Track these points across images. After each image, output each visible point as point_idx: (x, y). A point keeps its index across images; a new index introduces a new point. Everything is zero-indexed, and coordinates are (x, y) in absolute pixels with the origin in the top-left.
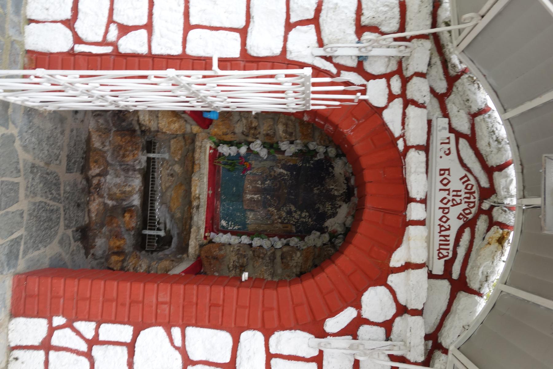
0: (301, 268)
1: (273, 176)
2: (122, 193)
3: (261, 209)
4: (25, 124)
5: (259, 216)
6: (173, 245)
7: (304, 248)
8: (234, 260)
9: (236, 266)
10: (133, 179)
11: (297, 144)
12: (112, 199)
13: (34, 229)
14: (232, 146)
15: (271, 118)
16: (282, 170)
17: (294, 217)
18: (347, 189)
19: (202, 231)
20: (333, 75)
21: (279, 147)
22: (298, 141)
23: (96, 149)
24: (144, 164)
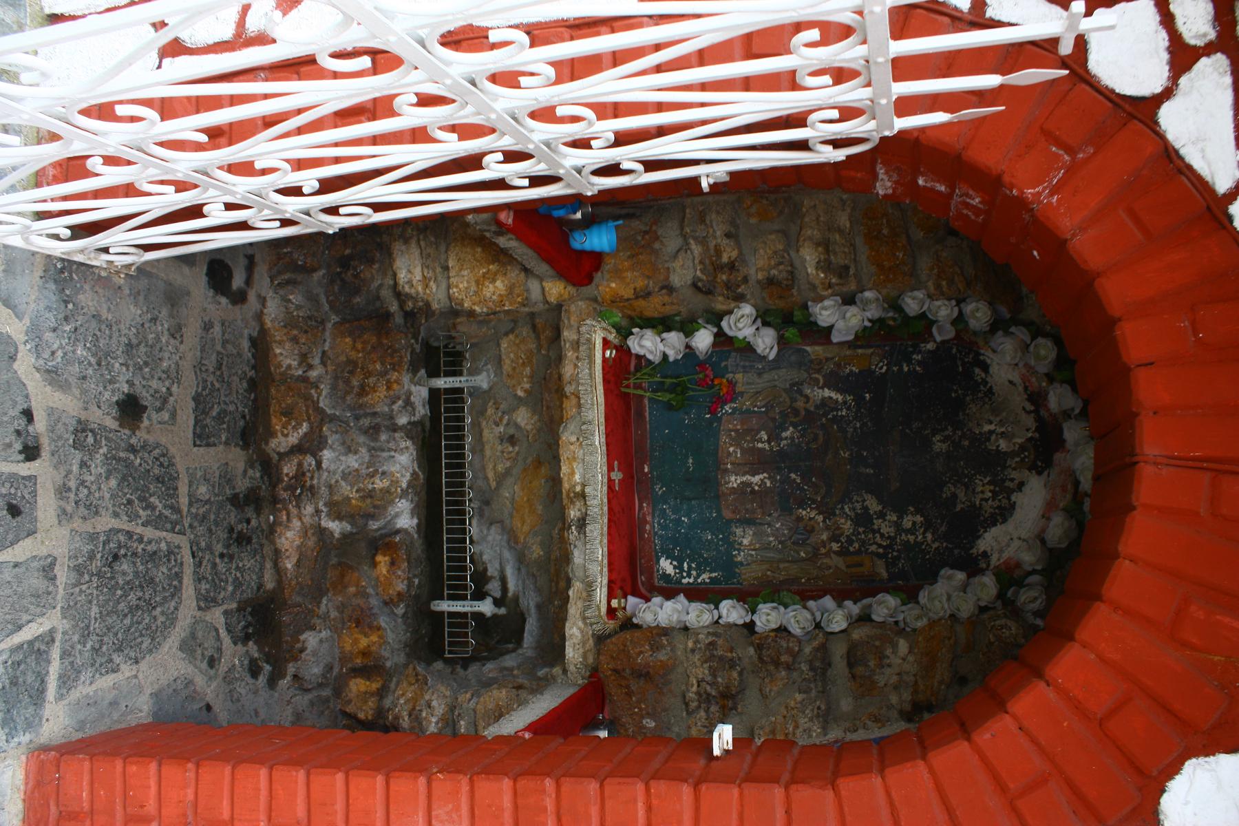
0: (915, 692)
1: (803, 413)
2: (363, 498)
3: (775, 515)
4: (49, 309)
5: (771, 539)
6: (528, 639)
7: (919, 624)
8: (700, 676)
9: (709, 695)
10: (392, 453)
11: (866, 302)
12: (339, 517)
13: (95, 610)
15: (778, 231)
16: (827, 393)
17: (879, 531)
18: (1037, 430)
19: (601, 594)
20: (959, 15)
21: (812, 319)
22: (868, 294)
23: (285, 377)
24: (422, 411)
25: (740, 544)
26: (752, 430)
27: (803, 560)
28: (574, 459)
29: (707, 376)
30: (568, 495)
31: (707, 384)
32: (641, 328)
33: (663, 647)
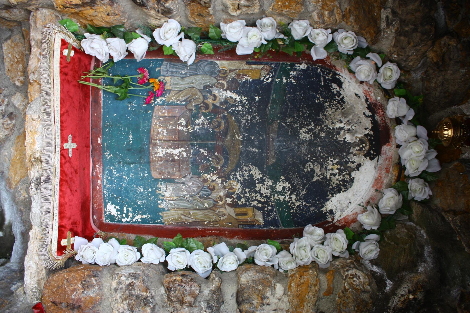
1: (211, 107)
3: (189, 177)
5: (185, 193)
11: (263, 26)
14: (114, 36)
16: (229, 94)
17: (259, 192)
18: (372, 129)
22: (266, 21)
25: (163, 196)
26: (175, 117)
27: (206, 209)
28: (36, 132)
29: (144, 76)
30: (30, 160)
31: (145, 82)
32: (91, 33)
33: (92, 286)
